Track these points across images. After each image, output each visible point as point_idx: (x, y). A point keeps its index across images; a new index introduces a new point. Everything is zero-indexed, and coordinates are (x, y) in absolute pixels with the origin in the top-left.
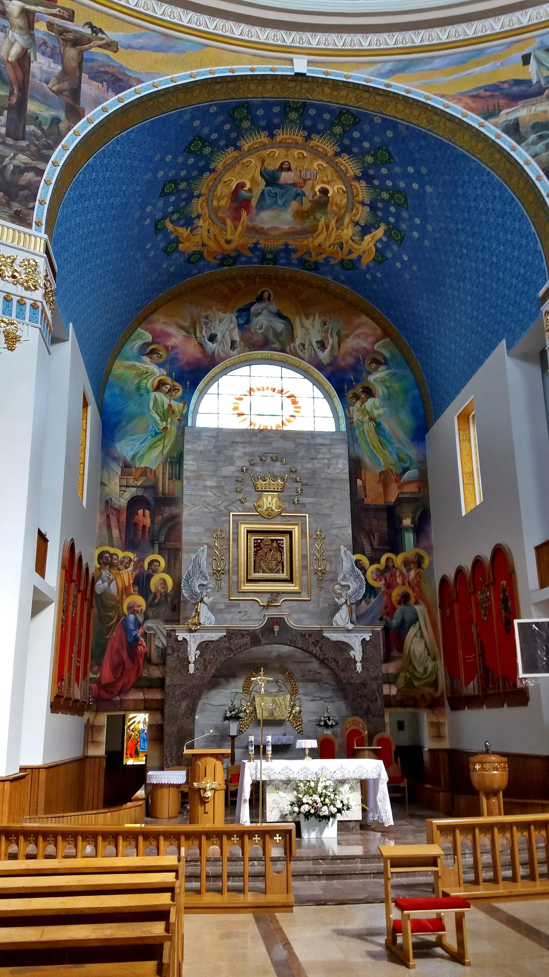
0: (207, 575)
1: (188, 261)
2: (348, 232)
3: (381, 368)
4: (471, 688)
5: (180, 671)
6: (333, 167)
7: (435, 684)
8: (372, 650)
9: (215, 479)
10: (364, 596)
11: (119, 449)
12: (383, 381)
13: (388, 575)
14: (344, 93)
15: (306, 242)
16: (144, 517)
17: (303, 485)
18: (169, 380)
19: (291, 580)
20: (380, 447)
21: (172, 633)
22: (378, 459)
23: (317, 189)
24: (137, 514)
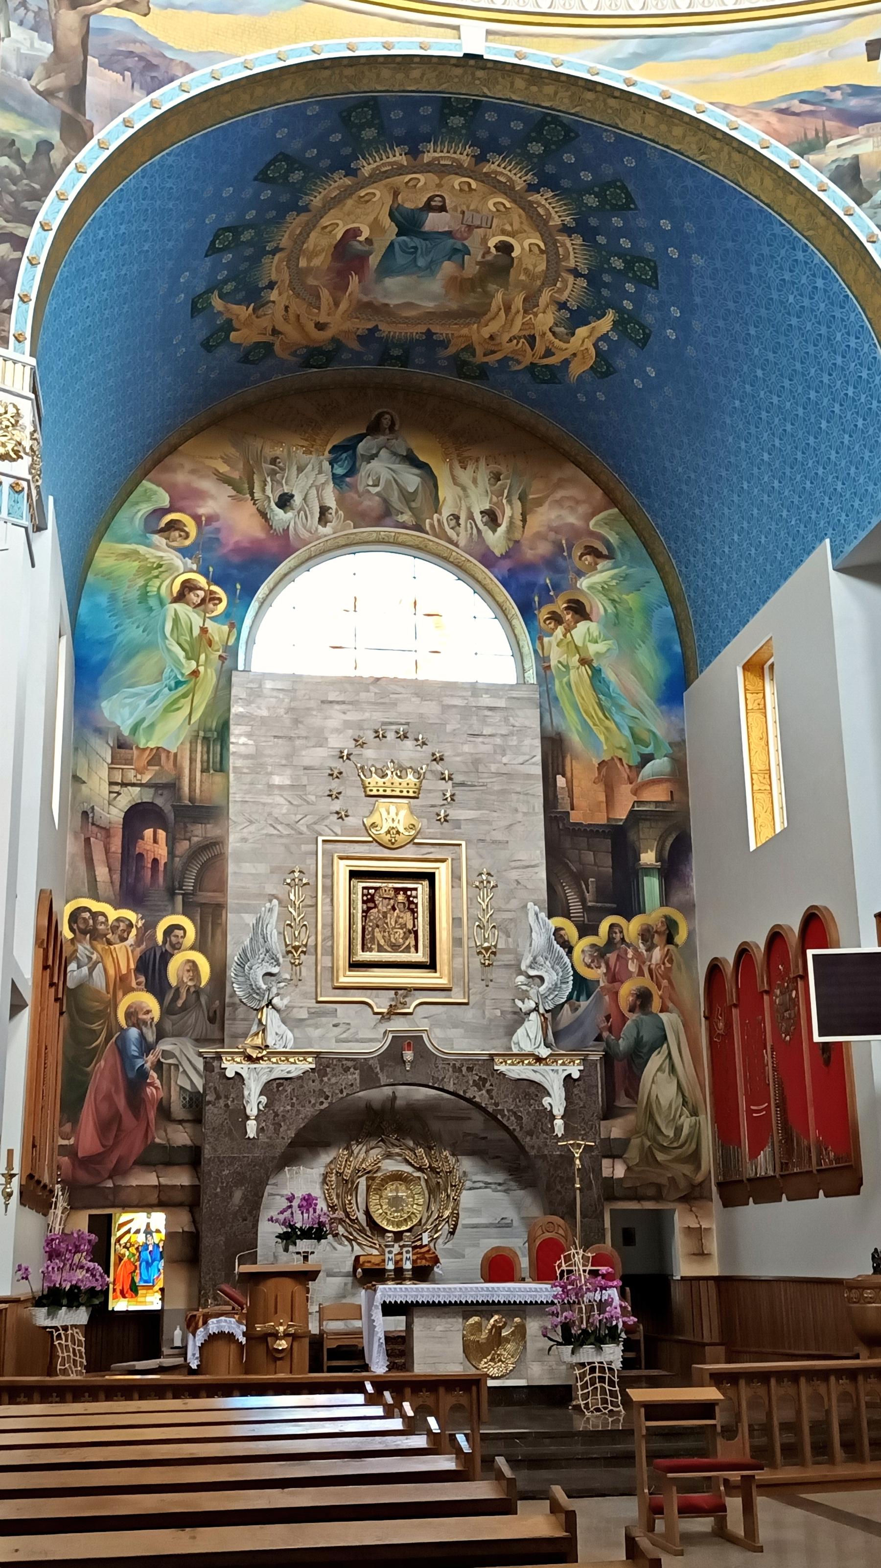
0: (280, 956)
1: (245, 359)
2: (545, 320)
3: (602, 564)
4: (763, 1164)
5: (229, 1134)
6: (523, 209)
7: (695, 1158)
8: (583, 1095)
9: (289, 772)
10: (570, 997)
11: (107, 714)
12: (605, 590)
13: (612, 957)
14: (549, 89)
15: (465, 331)
16: (155, 844)
17: (455, 785)
18: (202, 581)
19: (431, 965)
20: (601, 715)
21: (215, 1064)
22: (595, 740)
23: (492, 243)
24: (143, 839)
